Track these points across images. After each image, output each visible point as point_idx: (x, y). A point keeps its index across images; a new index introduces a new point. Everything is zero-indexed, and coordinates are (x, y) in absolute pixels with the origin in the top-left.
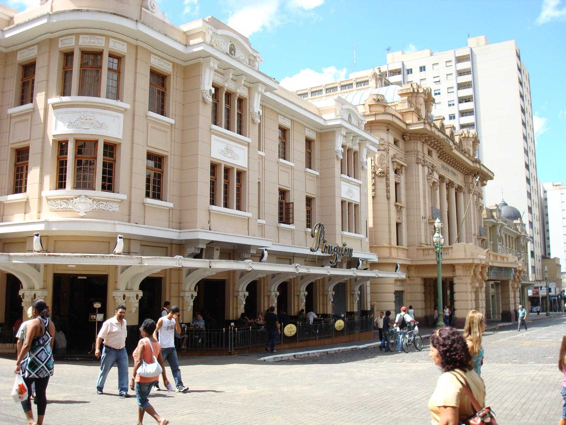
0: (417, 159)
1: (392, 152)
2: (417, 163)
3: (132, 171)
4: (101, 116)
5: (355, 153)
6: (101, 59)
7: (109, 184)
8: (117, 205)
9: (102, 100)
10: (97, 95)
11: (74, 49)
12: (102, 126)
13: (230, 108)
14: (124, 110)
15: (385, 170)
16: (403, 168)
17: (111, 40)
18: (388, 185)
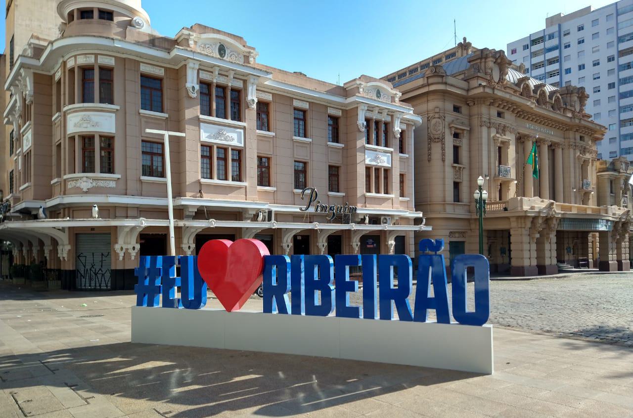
0: (481, 122)
1: (449, 118)
2: (481, 126)
3: (128, 157)
4: (95, 117)
5: (386, 124)
6: (93, 74)
7: (109, 168)
8: (114, 183)
9: (76, 105)
10: (93, 101)
11: (94, 65)
12: (97, 124)
13: (225, 99)
14: (115, 110)
15: (441, 136)
16: (465, 132)
17: (99, 56)
18: (443, 149)
